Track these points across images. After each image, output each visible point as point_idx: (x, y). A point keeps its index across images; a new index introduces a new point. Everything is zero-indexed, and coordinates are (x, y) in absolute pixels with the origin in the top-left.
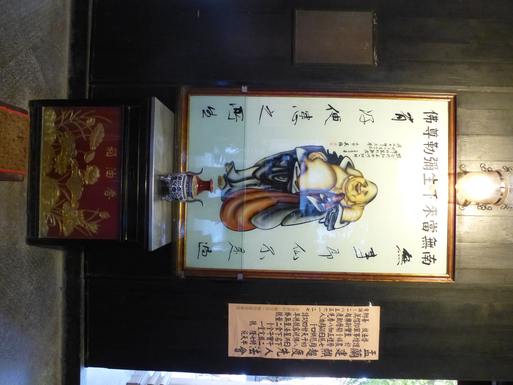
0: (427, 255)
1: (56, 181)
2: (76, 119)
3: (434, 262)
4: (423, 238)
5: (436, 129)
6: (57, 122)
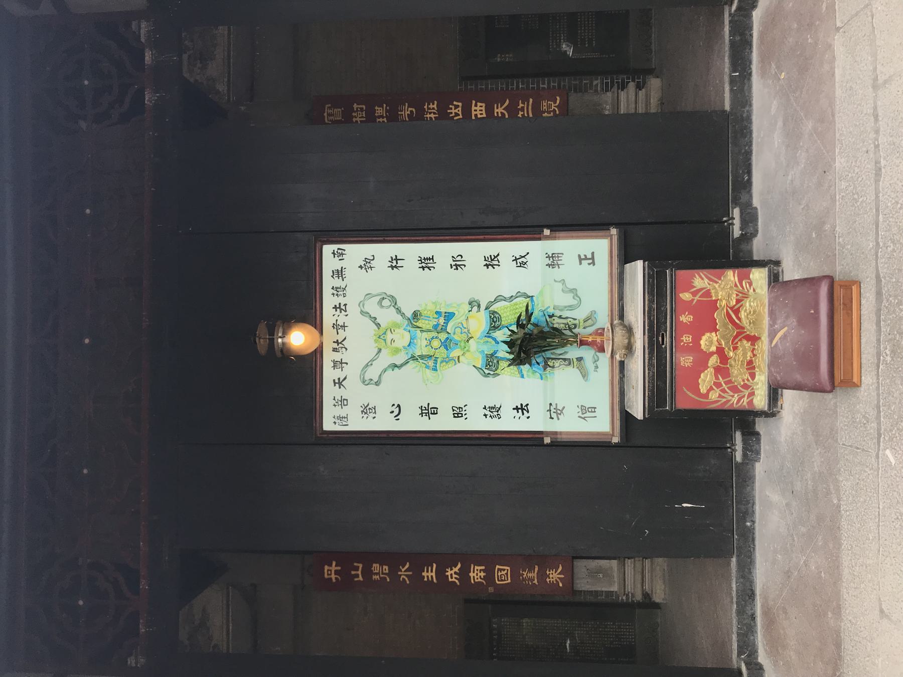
0: (341, 258)
1: (748, 333)
2: (730, 398)
3: (334, 251)
4: (345, 277)
5: (334, 369)
6: (752, 394)
